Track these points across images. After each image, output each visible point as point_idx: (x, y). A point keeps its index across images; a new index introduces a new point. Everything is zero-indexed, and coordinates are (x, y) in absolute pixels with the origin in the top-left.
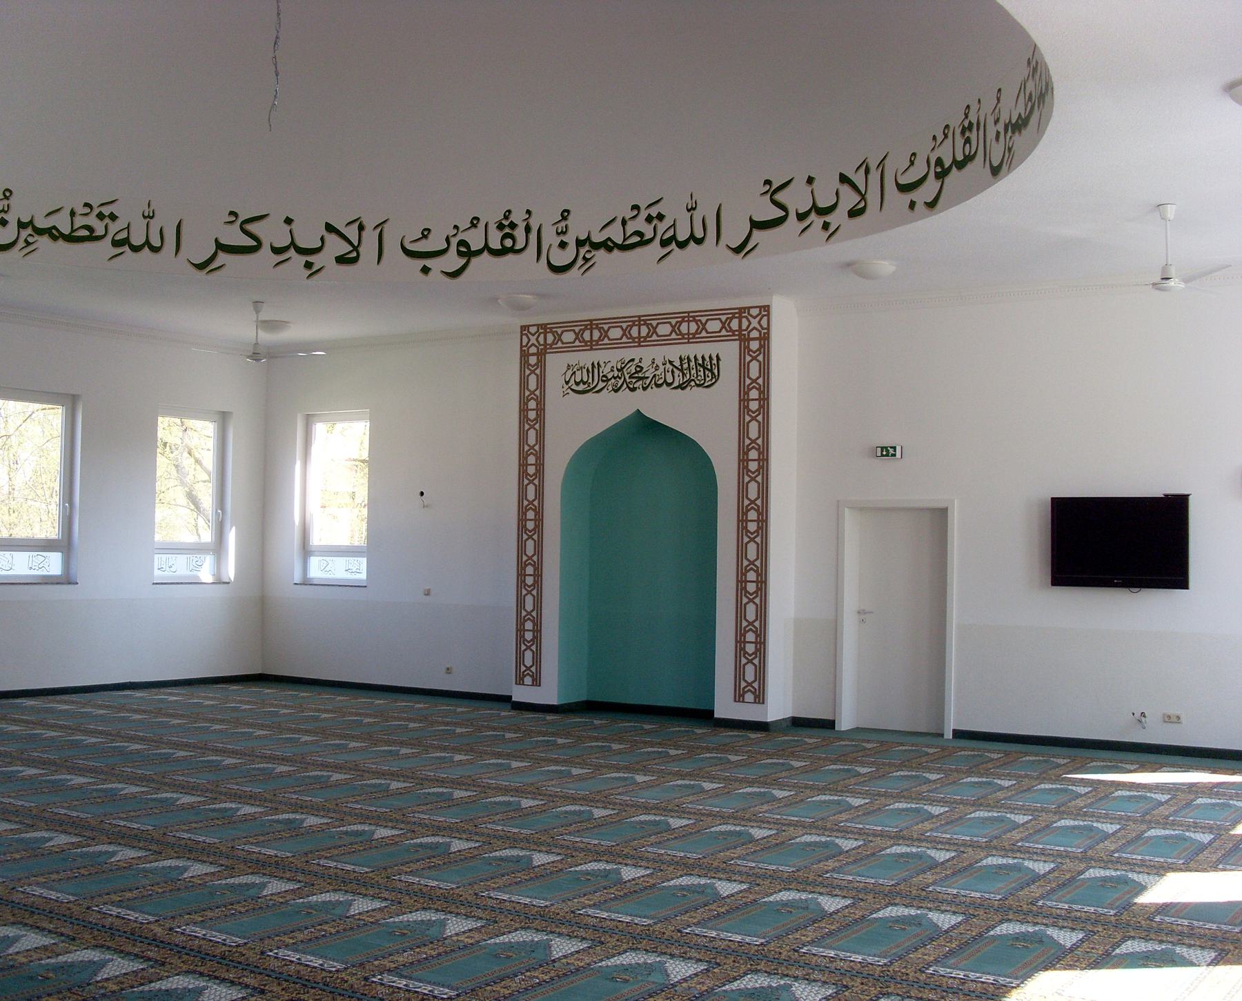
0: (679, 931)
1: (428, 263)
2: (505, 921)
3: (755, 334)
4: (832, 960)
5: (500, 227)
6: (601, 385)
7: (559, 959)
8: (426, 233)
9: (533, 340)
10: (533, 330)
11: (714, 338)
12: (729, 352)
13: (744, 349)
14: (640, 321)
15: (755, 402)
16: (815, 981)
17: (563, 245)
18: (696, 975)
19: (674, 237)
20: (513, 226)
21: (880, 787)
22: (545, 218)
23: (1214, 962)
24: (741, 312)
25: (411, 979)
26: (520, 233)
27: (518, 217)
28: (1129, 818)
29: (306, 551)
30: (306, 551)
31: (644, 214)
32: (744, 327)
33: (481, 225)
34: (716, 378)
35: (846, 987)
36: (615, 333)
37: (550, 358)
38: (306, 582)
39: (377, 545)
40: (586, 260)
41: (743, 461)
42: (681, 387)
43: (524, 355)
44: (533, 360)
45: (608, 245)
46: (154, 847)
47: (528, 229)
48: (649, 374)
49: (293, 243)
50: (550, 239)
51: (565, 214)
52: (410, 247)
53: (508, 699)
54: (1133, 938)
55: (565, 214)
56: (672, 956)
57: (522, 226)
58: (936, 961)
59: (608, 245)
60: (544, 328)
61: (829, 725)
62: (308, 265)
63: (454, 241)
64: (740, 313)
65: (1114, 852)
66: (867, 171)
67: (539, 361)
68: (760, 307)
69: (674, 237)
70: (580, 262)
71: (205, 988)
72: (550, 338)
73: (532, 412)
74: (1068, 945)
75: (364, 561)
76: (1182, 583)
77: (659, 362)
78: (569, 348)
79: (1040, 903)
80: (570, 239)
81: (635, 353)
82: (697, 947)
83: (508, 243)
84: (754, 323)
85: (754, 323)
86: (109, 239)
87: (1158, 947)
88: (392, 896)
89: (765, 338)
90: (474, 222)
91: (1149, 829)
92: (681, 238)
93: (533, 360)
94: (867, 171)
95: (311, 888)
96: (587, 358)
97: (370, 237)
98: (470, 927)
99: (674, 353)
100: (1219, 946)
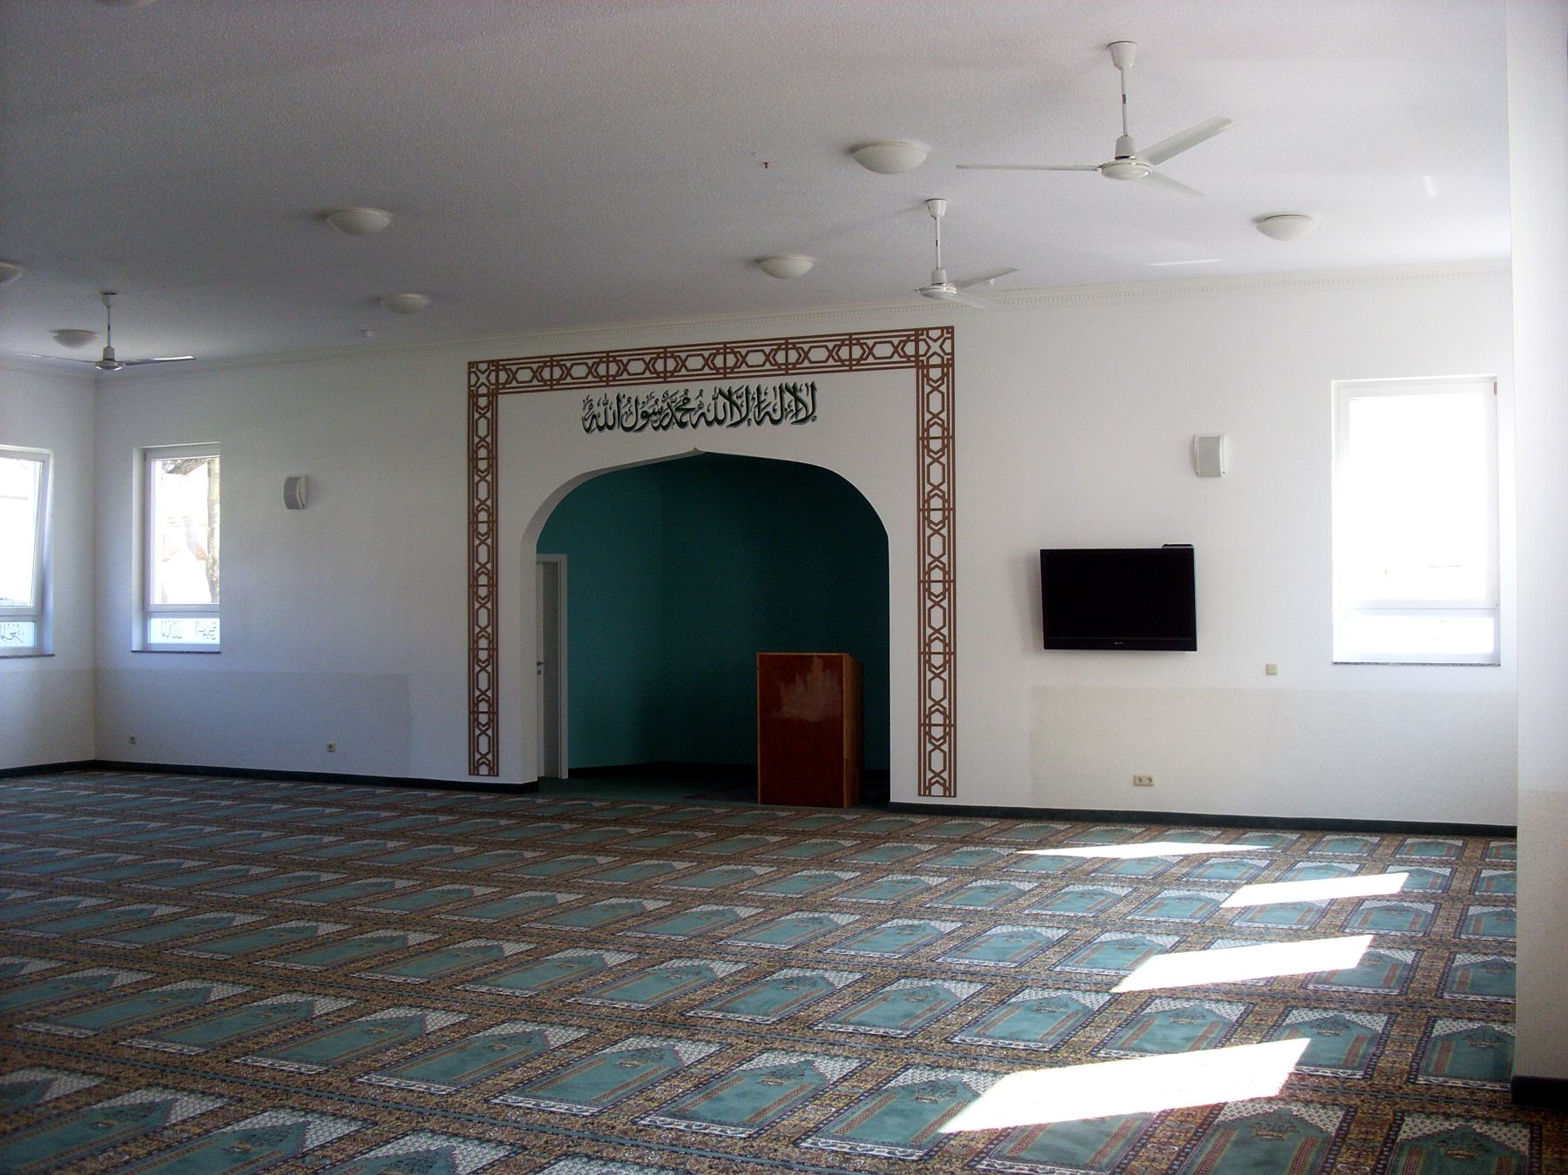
0: (486, 1101)
2: (389, 1121)
3: (935, 360)
6: (641, 422)
7: (313, 1150)
9: (483, 379)
10: (483, 367)
14: (787, 344)
15: (936, 439)
21: (869, 897)
23: (1219, 1108)
24: (918, 335)
29: (146, 612)
30: (146, 612)
32: (922, 352)
36: (695, 363)
37: (504, 401)
38: (146, 650)
39: (230, 604)
41: (924, 510)
43: (473, 396)
60: (496, 365)
64: (916, 335)
65: (1055, 965)
67: (490, 403)
68: (942, 329)
72: (503, 377)
73: (483, 458)
75: (217, 621)
76: (1192, 646)
79: (957, 1040)
84: (935, 347)
85: (935, 347)
88: (361, 1113)
89: (948, 365)
91: (1103, 932)
93: (483, 402)
98: (339, 1133)
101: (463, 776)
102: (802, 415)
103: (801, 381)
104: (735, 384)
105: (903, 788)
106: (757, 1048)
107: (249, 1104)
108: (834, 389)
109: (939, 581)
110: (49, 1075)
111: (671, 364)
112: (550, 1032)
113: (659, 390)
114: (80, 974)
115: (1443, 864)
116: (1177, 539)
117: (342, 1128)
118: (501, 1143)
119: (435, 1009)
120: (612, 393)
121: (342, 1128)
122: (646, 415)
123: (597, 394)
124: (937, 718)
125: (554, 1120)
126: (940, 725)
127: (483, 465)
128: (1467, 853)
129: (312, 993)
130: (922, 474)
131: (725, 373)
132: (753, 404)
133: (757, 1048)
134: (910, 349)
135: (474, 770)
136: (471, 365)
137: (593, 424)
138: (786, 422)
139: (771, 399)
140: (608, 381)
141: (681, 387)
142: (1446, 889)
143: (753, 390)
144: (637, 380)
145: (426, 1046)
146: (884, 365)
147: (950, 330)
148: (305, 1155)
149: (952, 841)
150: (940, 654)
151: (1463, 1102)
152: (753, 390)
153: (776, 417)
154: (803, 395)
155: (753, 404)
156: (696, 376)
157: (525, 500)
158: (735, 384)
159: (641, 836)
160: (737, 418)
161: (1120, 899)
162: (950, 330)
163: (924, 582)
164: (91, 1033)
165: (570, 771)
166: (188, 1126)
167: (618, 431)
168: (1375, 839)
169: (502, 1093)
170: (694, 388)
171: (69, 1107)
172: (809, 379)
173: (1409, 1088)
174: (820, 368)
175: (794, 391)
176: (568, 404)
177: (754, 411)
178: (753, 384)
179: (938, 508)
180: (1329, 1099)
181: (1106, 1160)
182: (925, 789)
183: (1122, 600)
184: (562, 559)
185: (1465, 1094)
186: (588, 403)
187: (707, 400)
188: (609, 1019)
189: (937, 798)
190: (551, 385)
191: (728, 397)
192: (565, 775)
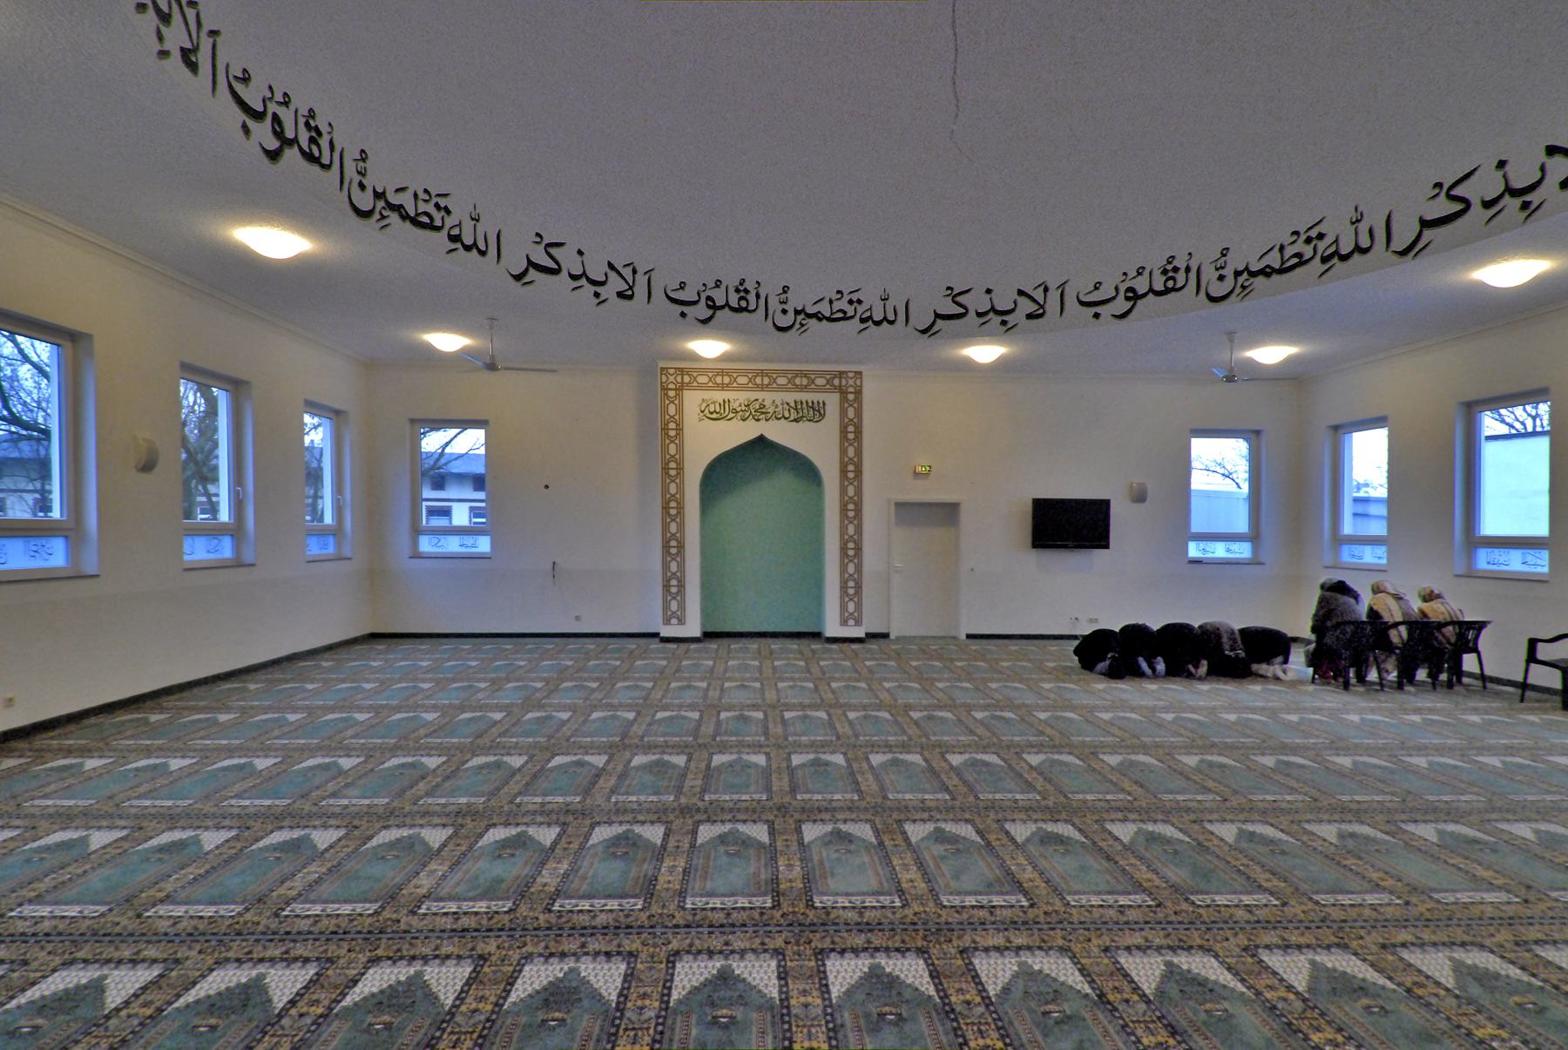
1: (686, 309)
4: (444, 806)
5: (737, 291)
7: (118, 1010)
8: (682, 286)
11: (820, 389)
12: (832, 401)
13: (844, 399)
15: (851, 433)
17: (1221, 278)
19: (870, 317)
20: (746, 291)
22: (771, 289)
26: (752, 297)
27: (750, 285)
31: (846, 298)
33: (723, 287)
34: (823, 416)
40: (1243, 287)
41: (843, 471)
42: (795, 420)
45: (818, 316)
47: (758, 296)
48: (771, 410)
49: (584, 274)
50: (774, 305)
51: (785, 289)
52: (672, 295)
53: (656, 635)
55: (785, 289)
56: (315, 827)
57: (753, 294)
58: (520, 793)
59: (818, 316)
61: (885, 636)
62: (597, 295)
63: (703, 296)
66: (1046, 290)
69: (870, 317)
70: (1238, 290)
72: (836, 382)
77: (778, 402)
78: (702, 387)
80: (1229, 272)
81: (760, 395)
82: (334, 816)
83: (743, 304)
86: (445, 232)
88: (26, 823)
90: (718, 284)
92: (876, 319)
94: (1046, 290)
95: (33, 831)
96: (719, 396)
97: (641, 281)
99: (791, 397)
106: (377, 826)
107: (35, 965)
109: (852, 510)
114: (42, 842)
116: (1029, 508)
117: (145, 975)
118: (154, 961)
119: (99, 828)
121: (145, 975)
124: (851, 591)
125: (344, 924)
130: (859, 452)
133: (377, 826)
134: (836, 382)
145: (207, 866)
147: (860, 373)
151: (731, 810)
164: (103, 909)
169: (288, 904)
171: (149, 1012)
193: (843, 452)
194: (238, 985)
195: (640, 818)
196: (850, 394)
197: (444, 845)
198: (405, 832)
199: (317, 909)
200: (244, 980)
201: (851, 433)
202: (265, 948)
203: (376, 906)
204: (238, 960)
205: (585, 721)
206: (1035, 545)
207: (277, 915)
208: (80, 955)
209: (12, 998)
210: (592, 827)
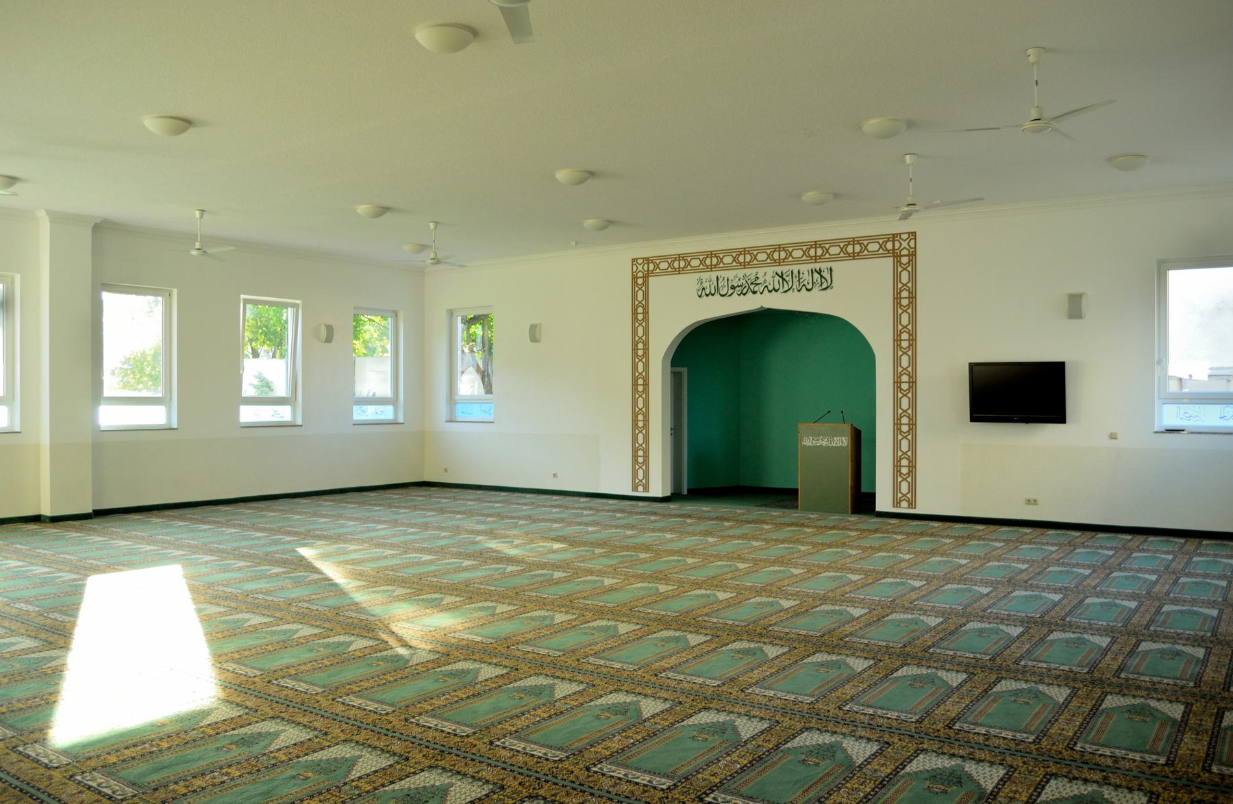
9: (640, 268)
15: (905, 299)
16: (861, 737)
18: (762, 732)
25: (528, 741)
28: (998, 582)
35: (887, 743)
36: (664, 266)
41: (897, 340)
43: (635, 278)
44: (640, 281)
46: (327, 625)
54: (1005, 678)
60: (648, 260)
71: (283, 731)
72: (889, 246)
73: (640, 313)
74: (955, 685)
84: (905, 244)
85: (905, 244)
87: (1025, 686)
88: (586, 679)
89: (913, 255)
93: (640, 281)
98: (573, 690)
100: (1072, 684)
101: (628, 492)
102: (824, 286)
103: (823, 266)
104: (785, 269)
105: (883, 503)
108: (843, 270)
109: (906, 383)
110: (353, 638)
111: (748, 258)
112: (690, 637)
113: (741, 273)
115: (1168, 553)
117: (575, 687)
120: (714, 275)
121: (575, 687)
122: (733, 287)
123: (705, 276)
126: (906, 467)
127: (640, 317)
128: (1186, 548)
129: (496, 601)
131: (779, 262)
132: (796, 280)
134: (889, 246)
135: (635, 488)
136: (633, 260)
137: (703, 293)
138: (815, 290)
139: (806, 277)
140: (711, 268)
141: (753, 271)
142: (1167, 568)
143: (796, 272)
144: (728, 267)
146: (874, 255)
147: (914, 234)
148: (644, 721)
149: (869, 531)
150: (906, 426)
151: (1147, 689)
152: (796, 272)
153: (809, 287)
154: (826, 274)
155: (796, 280)
156: (763, 264)
157: (665, 334)
158: (785, 269)
159: (731, 528)
160: (786, 288)
161: (1022, 571)
162: (914, 234)
163: (897, 383)
165: (689, 490)
166: (489, 683)
167: (717, 296)
168: (1182, 541)
170: (761, 271)
172: (829, 265)
173: (1114, 680)
174: (835, 258)
175: (819, 272)
176: (688, 282)
177: (796, 283)
178: (795, 268)
179: (906, 339)
180: (1173, 698)
181: (1032, 729)
182: (897, 503)
183: (1021, 394)
184: (684, 370)
185: (1148, 685)
186: (700, 280)
187: (769, 278)
188: (723, 629)
189: (904, 509)
190: (679, 271)
191: (819, 272)
192: (685, 492)
193: (897, 319)
194: (433, 786)
195: (978, 754)
196: (901, 253)
197: (868, 761)
198: (722, 717)
199: (620, 773)
200: (438, 784)
201: (905, 299)
202: (568, 794)
203: (670, 783)
204: (444, 769)
205: (1131, 653)
206: (973, 419)
207: (588, 769)
208: (441, 763)
209: (392, 782)
210: (917, 752)
